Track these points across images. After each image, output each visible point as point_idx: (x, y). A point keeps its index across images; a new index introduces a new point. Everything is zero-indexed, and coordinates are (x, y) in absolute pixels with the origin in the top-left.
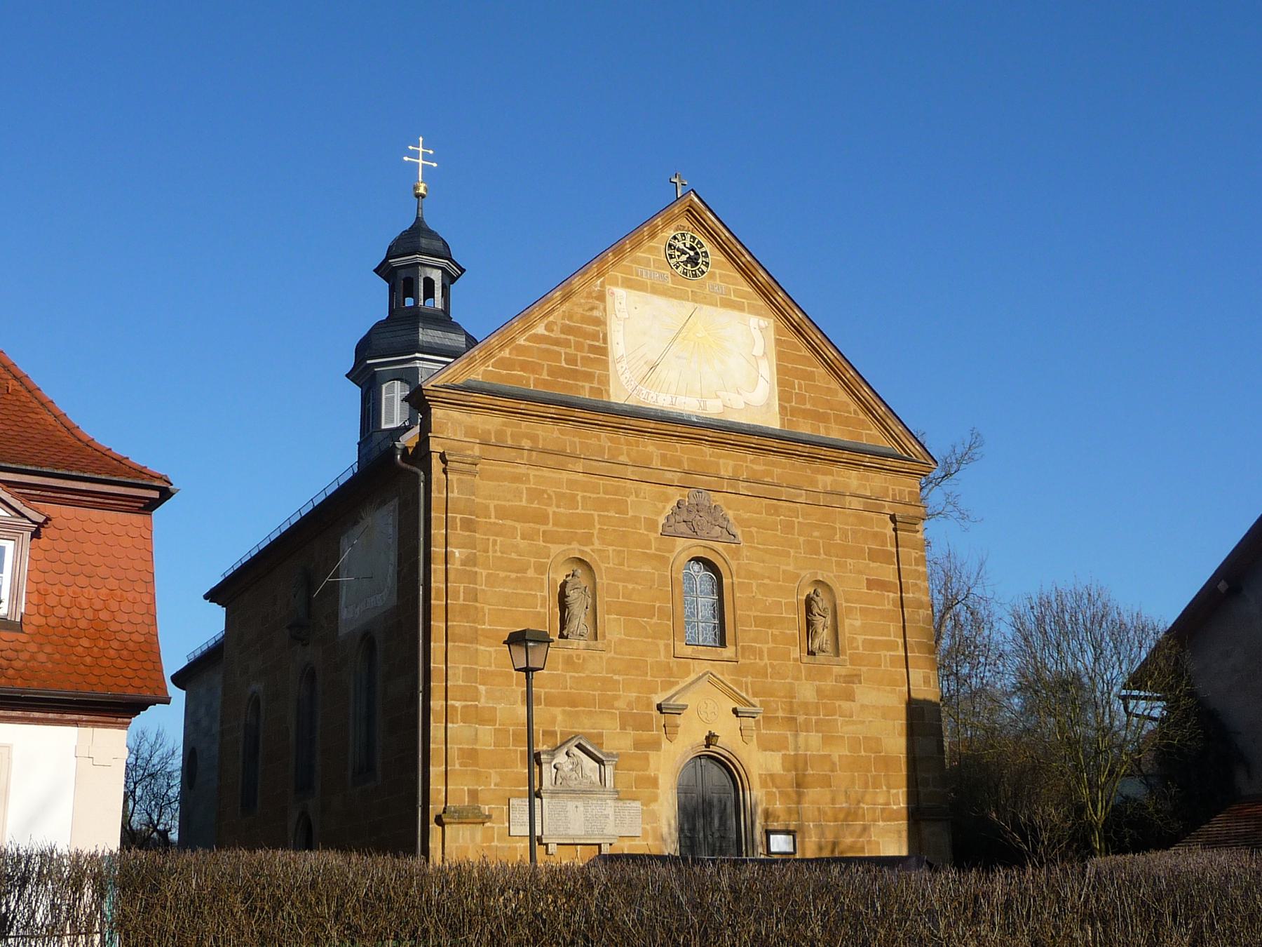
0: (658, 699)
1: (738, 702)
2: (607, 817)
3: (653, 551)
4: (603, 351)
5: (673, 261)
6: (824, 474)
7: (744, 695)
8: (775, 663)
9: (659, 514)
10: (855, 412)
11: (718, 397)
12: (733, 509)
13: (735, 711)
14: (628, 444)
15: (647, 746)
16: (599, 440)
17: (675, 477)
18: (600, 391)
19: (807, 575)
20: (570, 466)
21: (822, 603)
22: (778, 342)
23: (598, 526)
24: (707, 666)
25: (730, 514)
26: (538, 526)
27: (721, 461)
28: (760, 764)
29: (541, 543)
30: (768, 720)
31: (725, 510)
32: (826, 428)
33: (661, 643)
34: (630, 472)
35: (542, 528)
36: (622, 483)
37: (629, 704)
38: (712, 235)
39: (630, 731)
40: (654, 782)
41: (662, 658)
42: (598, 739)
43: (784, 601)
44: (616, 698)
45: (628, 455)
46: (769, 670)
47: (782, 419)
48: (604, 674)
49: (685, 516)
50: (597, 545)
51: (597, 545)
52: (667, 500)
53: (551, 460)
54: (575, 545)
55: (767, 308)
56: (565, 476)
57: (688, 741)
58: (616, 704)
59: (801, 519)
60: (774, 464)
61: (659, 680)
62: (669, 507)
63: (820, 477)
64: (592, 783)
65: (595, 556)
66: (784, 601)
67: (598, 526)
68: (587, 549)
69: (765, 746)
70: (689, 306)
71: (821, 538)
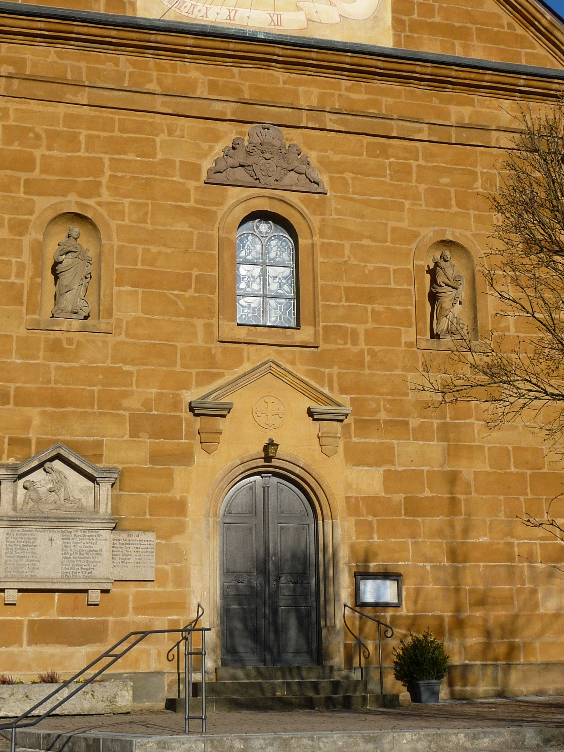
0: (191, 395)
1: (317, 400)
2: (98, 553)
3: (192, 204)
6: (459, 104)
7: (326, 391)
8: (376, 348)
9: (204, 156)
10: (510, 26)
11: (299, 9)
12: (316, 151)
13: (310, 413)
14: (161, 69)
15: (169, 459)
16: (117, 65)
17: (229, 110)
19: (429, 234)
20: (69, 97)
21: (454, 268)
23: (108, 173)
24: (269, 353)
25: (313, 156)
26: (16, 174)
27: (301, 89)
28: (344, 479)
29: (22, 195)
30: (364, 425)
31: (305, 150)
32: (465, 47)
33: (199, 323)
34: (159, 104)
35: (24, 176)
36: (148, 118)
37: (146, 404)
39: (146, 440)
40: (180, 507)
41: (200, 342)
42: (94, 451)
43: (392, 267)
44: (126, 395)
45: (160, 83)
46: (367, 358)
47: (397, 36)
48: (108, 363)
49: (240, 157)
50: (106, 195)
51: (106, 195)
52: (217, 138)
53: (40, 90)
54: (73, 197)
56: (61, 109)
57: (240, 440)
58: (126, 403)
59: (421, 162)
60: (382, 92)
61: (194, 371)
62: (218, 149)
63: (453, 108)
64: (82, 509)
65: (102, 211)
66: (392, 267)
67: (108, 173)
68: (91, 202)
69: (356, 457)
71: (453, 185)
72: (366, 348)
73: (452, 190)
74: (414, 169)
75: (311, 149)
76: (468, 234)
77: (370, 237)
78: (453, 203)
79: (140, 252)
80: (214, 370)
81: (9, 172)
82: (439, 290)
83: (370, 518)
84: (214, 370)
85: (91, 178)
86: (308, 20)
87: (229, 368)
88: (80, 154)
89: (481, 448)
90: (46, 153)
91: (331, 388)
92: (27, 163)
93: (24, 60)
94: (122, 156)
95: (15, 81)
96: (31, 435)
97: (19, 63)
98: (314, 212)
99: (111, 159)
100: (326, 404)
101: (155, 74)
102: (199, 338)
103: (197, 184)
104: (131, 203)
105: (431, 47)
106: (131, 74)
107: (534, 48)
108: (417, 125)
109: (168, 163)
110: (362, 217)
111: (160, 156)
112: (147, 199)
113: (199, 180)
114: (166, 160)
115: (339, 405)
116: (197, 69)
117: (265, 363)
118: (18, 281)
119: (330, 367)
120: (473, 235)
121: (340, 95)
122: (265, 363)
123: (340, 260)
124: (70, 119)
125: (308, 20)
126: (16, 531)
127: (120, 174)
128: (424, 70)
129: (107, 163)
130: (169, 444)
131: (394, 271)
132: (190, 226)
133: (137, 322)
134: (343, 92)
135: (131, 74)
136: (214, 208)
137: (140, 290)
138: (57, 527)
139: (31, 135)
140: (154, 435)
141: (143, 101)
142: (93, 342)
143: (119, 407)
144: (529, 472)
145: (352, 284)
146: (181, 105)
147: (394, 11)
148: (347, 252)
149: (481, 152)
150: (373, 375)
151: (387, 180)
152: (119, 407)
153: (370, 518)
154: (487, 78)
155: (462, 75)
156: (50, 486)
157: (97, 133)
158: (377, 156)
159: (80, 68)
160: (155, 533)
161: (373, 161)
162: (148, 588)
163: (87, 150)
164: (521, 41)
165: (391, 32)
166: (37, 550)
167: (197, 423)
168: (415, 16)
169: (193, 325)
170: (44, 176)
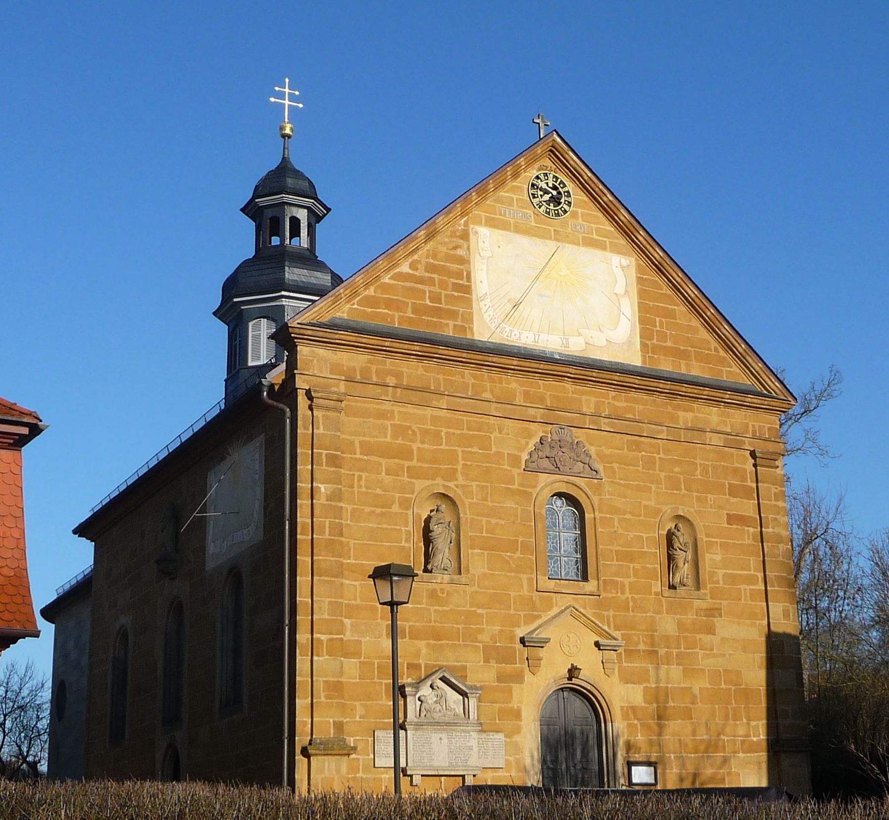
0: (521, 632)
1: (600, 635)
2: (471, 748)
3: (516, 487)
4: (467, 289)
5: (535, 201)
6: (685, 410)
7: (606, 628)
8: (636, 597)
9: (522, 449)
11: (580, 335)
12: (596, 445)
13: (597, 644)
14: (492, 381)
17: (538, 414)
18: (463, 329)
19: (668, 510)
21: (683, 537)
22: (640, 280)
23: (461, 462)
24: (569, 600)
25: (593, 450)
26: (402, 462)
27: (584, 397)
28: (621, 696)
29: (406, 478)
32: (688, 366)
33: (524, 577)
34: (493, 409)
35: (407, 464)
37: (492, 638)
38: (575, 175)
39: (493, 663)
41: (525, 591)
44: (480, 631)
45: (492, 392)
46: (631, 604)
47: (644, 357)
48: (468, 608)
50: (461, 481)
51: (461, 481)
52: (530, 436)
53: (415, 397)
55: (629, 247)
56: (429, 412)
58: (480, 637)
59: (662, 455)
60: (635, 400)
61: (522, 614)
63: (681, 414)
65: (459, 491)
66: (645, 536)
68: (451, 485)
69: (627, 678)
70: (552, 244)
72: (630, 596)
73: (682, 477)
74: (657, 460)
75: (592, 445)
76: (692, 510)
77: (630, 513)
78: (683, 487)
79: (484, 523)
80: (535, 613)
81: (396, 461)
82: (675, 552)
83: (636, 722)
84: (535, 613)
85: (450, 466)
86: (586, 343)
87: (546, 611)
88: (442, 447)
89: (703, 670)
90: (421, 446)
91: (609, 627)
92: (407, 454)
93: (402, 373)
94: (470, 449)
95: (399, 390)
96: (422, 662)
97: (398, 375)
98: (594, 494)
99: (463, 451)
100: (607, 638)
101: (488, 384)
102: (620, 712)
103: (519, 471)
104: (477, 486)
105: (666, 366)
106: (473, 384)
107: (731, 367)
108: (660, 427)
109: (499, 454)
110: (625, 497)
111: (494, 449)
112: (487, 482)
113: (520, 468)
114: (499, 452)
115: (616, 639)
116: (516, 381)
117: (568, 608)
118: (407, 545)
119: (608, 610)
120: (696, 511)
121: (609, 403)
122: (568, 608)
123: (612, 530)
124: (435, 420)
125: (586, 343)
126: (418, 733)
127: (469, 463)
128: (665, 387)
129: (460, 454)
130: (508, 668)
131: (647, 538)
132: (516, 504)
133: (485, 575)
134: (610, 401)
135: (473, 384)
136: (530, 490)
137: (486, 553)
138: (444, 730)
139: (410, 432)
140: (499, 662)
141: (482, 407)
142: (457, 591)
143: (476, 640)
144: (733, 688)
145: (621, 548)
146: (507, 410)
147: (641, 337)
148: (616, 524)
149: (701, 449)
150: (635, 616)
151: (640, 469)
152: (476, 640)
153: (636, 722)
154: (705, 393)
155: (690, 390)
156: (435, 699)
157: (452, 431)
158: (634, 451)
159: (439, 379)
160: (534, 779)
161: (632, 454)
162: (500, 773)
163: (447, 445)
164: (722, 360)
165: (640, 353)
166: (432, 746)
167: (525, 652)
168: (655, 341)
169: (520, 579)
170: (419, 464)
